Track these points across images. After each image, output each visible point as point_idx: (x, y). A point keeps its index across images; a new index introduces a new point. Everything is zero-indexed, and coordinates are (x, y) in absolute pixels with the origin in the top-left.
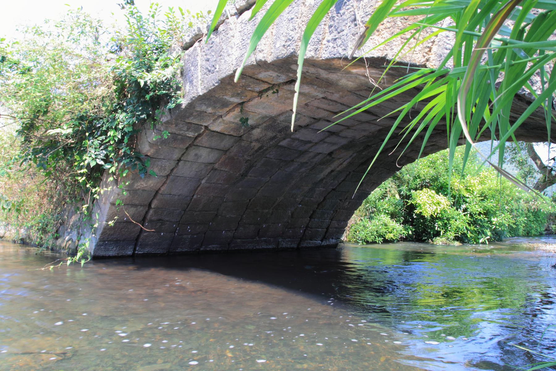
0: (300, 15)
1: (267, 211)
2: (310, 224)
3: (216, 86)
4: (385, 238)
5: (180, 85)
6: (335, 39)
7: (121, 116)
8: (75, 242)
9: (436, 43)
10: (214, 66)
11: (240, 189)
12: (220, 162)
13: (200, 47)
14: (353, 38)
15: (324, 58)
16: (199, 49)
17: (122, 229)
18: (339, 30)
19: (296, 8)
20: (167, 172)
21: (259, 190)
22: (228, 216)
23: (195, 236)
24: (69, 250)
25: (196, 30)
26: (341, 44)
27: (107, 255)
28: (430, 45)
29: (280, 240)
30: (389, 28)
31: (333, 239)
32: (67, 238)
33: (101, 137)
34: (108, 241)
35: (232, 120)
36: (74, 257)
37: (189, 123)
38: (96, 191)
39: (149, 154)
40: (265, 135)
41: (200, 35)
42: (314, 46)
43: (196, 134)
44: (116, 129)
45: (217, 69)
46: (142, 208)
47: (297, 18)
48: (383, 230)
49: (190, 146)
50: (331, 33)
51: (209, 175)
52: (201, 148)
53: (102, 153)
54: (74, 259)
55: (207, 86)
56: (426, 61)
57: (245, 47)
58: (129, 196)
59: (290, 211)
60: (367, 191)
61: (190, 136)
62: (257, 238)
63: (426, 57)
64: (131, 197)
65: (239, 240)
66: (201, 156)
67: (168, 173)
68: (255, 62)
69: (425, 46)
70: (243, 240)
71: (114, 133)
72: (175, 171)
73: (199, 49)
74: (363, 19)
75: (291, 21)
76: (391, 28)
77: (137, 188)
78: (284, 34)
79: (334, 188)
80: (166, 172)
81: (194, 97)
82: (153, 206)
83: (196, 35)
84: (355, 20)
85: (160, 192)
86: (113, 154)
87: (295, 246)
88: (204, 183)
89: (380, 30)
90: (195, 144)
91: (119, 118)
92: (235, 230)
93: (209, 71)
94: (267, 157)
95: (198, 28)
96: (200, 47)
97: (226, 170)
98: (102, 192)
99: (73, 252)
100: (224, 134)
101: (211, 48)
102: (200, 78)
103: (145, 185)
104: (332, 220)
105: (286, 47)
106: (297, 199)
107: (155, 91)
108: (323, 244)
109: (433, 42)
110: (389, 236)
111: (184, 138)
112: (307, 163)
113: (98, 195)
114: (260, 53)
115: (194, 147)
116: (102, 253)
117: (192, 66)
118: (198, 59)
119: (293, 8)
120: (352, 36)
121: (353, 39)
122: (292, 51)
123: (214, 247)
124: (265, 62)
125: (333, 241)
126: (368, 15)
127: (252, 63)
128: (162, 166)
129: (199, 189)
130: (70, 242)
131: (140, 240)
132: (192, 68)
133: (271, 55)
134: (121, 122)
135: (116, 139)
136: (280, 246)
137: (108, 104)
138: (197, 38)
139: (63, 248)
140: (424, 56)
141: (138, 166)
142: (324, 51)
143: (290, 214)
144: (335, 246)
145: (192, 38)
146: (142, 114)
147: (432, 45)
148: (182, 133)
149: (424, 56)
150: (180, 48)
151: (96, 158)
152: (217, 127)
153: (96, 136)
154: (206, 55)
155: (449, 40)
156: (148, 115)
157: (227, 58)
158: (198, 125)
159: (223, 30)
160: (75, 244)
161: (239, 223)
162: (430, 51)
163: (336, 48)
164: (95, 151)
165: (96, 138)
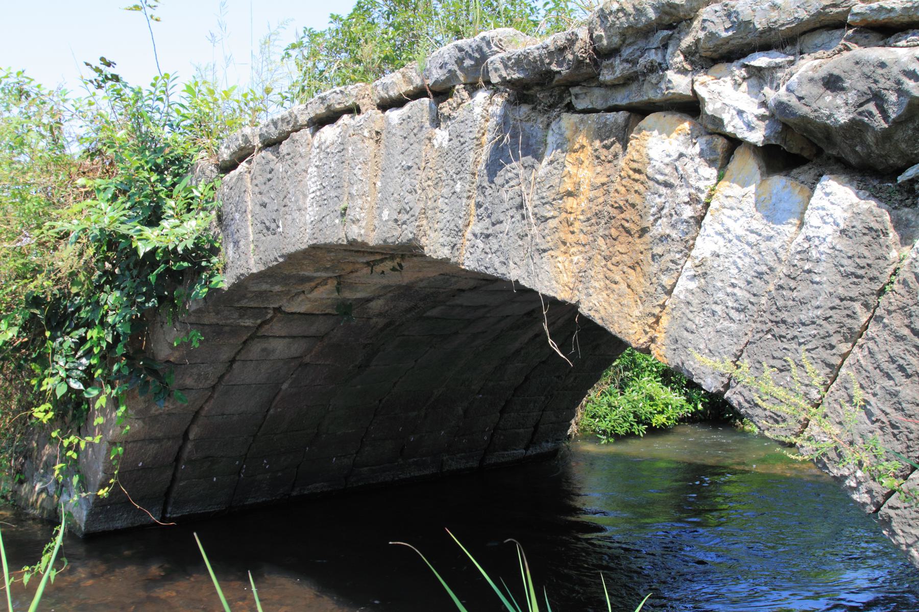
0: (423, 164)
1: (415, 413)
2: (501, 423)
3: (281, 263)
4: (650, 425)
5: (217, 245)
6: (488, 236)
7: (111, 298)
8: (52, 497)
9: (667, 310)
10: (274, 220)
11: (359, 387)
12: (313, 353)
13: (250, 172)
14: (520, 243)
15: (467, 268)
16: (248, 177)
17: (135, 481)
18: (494, 219)
19: (416, 145)
20: (211, 382)
21: (395, 383)
22: (339, 433)
23: (280, 474)
24: (43, 512)
25: (240, 139)
26: (498, 251)
27: (111, 529)
28: (657, 311)
29: (445, 458)
30: (584, 245)
31: (547, 442)
32: (38, 487)
33: (76, 332)
34: (111, 505)
35: (325, 296)
36: (35, 564)
37: (241, 308)
38: (71, 443)
39: (172, 359)
40: (394, 307)
41: (249, 149)
42: (450, 238)
43: (259, 321)
44: (103, 324)
45: (280, 230)
46: (170, 443)
47: (419, 169)
48: (645, 408)
49: (251, 338)
50: (480, 218)
51: (294, 376)
52: (271, 340)
53: (81, 364)
54: (36, 567)
55: (264, 258)
56: (649, 342)
57: (326, 202)
58: (143, 427)
59: (460, 408)
60: (609, 355)
61: (246, 325)
62: (400, 460)
63: (650, 334)
64: (147, 427)
65: (366, 469)
66: (274, 351)
67: (213, 383)
68: (346, 241)
69: (648, 311)
70: (374, 468)
71: (99, 333)
72: (226, 378)
73: (248, 177)
74: (536, 210)
75: (408, 172)
76: (587, 247)
77: (157, 413)
78: (395, 195)
79: (544, 359)
80: (209, 382)
81: (242, 275)
82: (191, 437)
83: (241, 149)
84: (521, 206)
85: (203, 413)
86: (100, 371)
87: (475, 464)
88: (286, 389)
89: (568, 244)
90: (259, 334)
91: (106, 303)
92: (357, 453)
93: (268, 229)
94: (404, 335)
95: (243, 135)
96: (250, 172)
97: (328, 362)
98: (83, 445)
99: (49, 516)
100: (313, 314)
101: (269, 180)
102: (251, 238)
103: (171, 407)
104: (543, 410)
105: (399, 223)
106: (473, 387)
107: (167, 262)
108: (529, 452)
109: (663, 306)
110: (658, 420)
111: (235, 330)
112: (483, 332)
113: (75, 451)
114: (354, 226)
115: (257, 340)
116: (100, 527)
117: (236, 211)
118: (246, 200)
119: (411, 144)
120: (517, 238)
121: (520, 246)
122: (411, 236)
123: (317, 488)
124: (364, 244)
125: (548, 446)
126: (546, 203)
127: (340, 241)
128: (199, 375)
129: (278, 398)
130: (44, 495)
131: (174, 494)
132: (237, 216)
133: (374, 230)
134: (112, 310)
135: (104, 345)
136: (446, 469)
137: (83, 279)
138: (243, 154)
139: (32, 505)
140: (646, 333)
141: (152, 387)
142: (468, 255)
143: (461, 412)
144: (554, 453)
145: (234, 153)
146: (148, 300)
147: (661, 312)
148: (232, 323)
149: (646, 333)
150: (213, 168)
151: (68, 377)
152: (299, 306)
153: (69, 330)
154: (260, 193)
155: (691, 312)
156: (161, 299)
157: (296, 215)
158: (260, 308)
159: (289, 154)
160: (53, 501)
161: (362, 441)
162: (657, 322)
163: (490, 256)
164: (67, 362)
165: (68, 334)
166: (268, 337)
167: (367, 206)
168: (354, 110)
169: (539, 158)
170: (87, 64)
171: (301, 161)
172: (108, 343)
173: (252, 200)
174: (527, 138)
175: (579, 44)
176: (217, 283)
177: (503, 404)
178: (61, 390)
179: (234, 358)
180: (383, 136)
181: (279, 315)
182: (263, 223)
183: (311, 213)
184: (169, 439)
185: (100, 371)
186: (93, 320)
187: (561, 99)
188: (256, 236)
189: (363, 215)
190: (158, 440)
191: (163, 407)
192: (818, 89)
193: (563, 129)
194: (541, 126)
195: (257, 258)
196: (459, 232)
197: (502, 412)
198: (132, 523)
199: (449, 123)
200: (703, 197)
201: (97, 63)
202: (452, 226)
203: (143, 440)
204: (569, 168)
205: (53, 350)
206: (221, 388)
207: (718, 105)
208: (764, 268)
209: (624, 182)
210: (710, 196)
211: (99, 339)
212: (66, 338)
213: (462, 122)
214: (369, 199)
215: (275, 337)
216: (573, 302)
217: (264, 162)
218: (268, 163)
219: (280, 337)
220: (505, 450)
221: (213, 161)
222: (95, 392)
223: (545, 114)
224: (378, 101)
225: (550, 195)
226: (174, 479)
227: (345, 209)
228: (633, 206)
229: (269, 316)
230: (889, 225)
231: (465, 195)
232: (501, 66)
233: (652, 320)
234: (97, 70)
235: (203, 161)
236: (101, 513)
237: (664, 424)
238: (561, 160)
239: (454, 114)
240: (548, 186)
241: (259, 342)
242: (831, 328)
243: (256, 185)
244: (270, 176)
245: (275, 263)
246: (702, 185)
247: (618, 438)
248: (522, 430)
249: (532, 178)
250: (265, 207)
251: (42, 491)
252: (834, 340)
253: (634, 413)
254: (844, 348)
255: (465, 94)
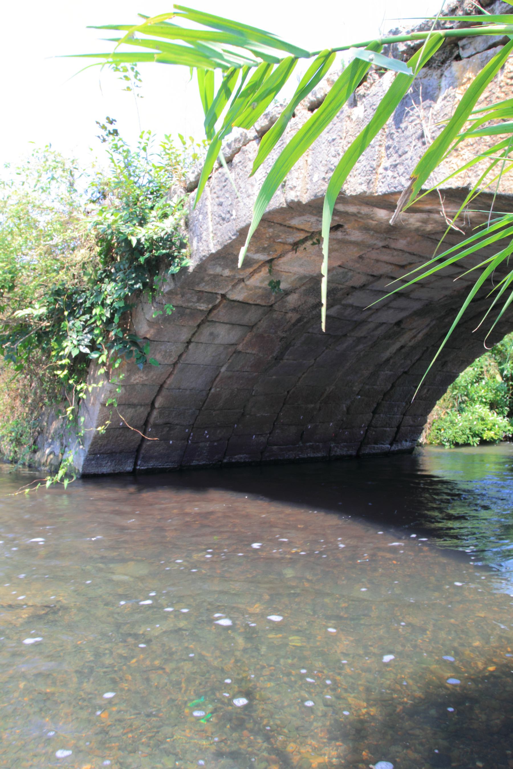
0: (344, 135)
1: (312, 406)
5: (185, 241)
6: (395, 166)
7: (109, 287)
10: (229, 212)
12: (245, 342)
17: (117, 437)
18: (400, 152)
20: (173, 359)
21: (300, 378)
22: (258, 415)
23: (216, 444)
26: (404, 172)
27: (100, 473)
29: (332, 445)
30: (472, 145)
31: (406, 441)
32: (48, 451)
34: (100, 454)
35: (258, 284)
37: (200, 291)
38: (82, 388)
40: (305, 302)
43: (210, 306)
44: (103, 305)
45: (234, 217)
47: (341, 138)
48: (478, 427)
49: (203, 322)
50: (388, 156)
51: (230, 361)
52: (217, 324)
54: (55, 478)
55: (221, 240)
59: (344, 405)
62: (300, 443)
64: (127, 394)
65: (276, 447)
66: (218, 336)
67: (175, 361)
71: (101, 311)
72: (184, 357)
75: (332, 143)
76: (475, 145)
77: (135, 382)
79: (406, 370)
80: (172, 359)
81: (204, 256)
82: (157, 405)
84: (422, 136)
85: (166, 386)
87: (353, 452)
88: (224, 372)
90: (209, 318)
91: (106, 290)
92: (270, 433)
93: (223, 219)
94: (309, 333)
100: (248, 304)
101: (224, 187)
102: (211, 229)
103: (145, 378)
105: (326, 180)
106: (354, 389)
107: (151, 251)
110: (487, 435)
111: (194, 313)
112: (365, 337)
115: (207, 323)
116: (93, 470)
119: (335, 124)
123: (241, 458)
124: (299, 203)
125: (406, 445)
127: (281, 205)
128: (166, 352)
129: (218, 379)
130: (52, 456)
131: (143, 451)
132: (201, 217)
135: (104, 319)
136: (333, 453)
137: (91, 272)
139: (44, 464)
141: (134, 353)
142: (381, 184)
143: (345, 409)
144: (410, 451)
146: (136, 283)
150: (182, 190)
153: (78, 316)
154: (218, 197)
156: (145, 284)
159: (240, 162)
161: (274, 424)
163: (398, 178)
165: (78, 318)
166: (216, 322)
167: (301, 176)
169: (434, 99)
170: (97, 123)
172: (107, 317)
173: (211, 204)
174: (425, 89)
176: (187, 263)
177: (375, 405)
179: (190, 340)
181: (225, 301)
182: (220, 216)
184: (141, 405)
185: (101, 339)
186: (97, 302)
187: (451, 53)
188: (215, 227)
189: (298, 183)
190: (133, 406)
191: (138, 378)
193: (454, 72)
194: (436, 77)
195: (215, 242)
197: (374, 412)
198: (114, 470)
199: (364, 100)
201: (104, 122)
202: (368, 168)
203: (124, 404)
206: (179, 365)
209: (503, 90)
211: (101, 315)
212: (76, 320)
213: (374, 95)
214: (303, 171)
216: (465, 185)
217: (220, 176)
220: (376, 443)
221: (182, 184)
223: (438, 69)
224: (309, 105)
229: (218, 301)
231: (378, 143)
234: (104, 127)
236: (93, 460)
237: (492, 438)
238: (452, 94)
239: (368, 92)
240: (442, 115)
241: (208, 326)
243: (215, 193)
245: (229, 241)
247: (457, 445)
248: (388, 429)
249: (430, 114)
250: (221, 205)
251: (50, 453)
253: (470, 429)
255: (376, 76)
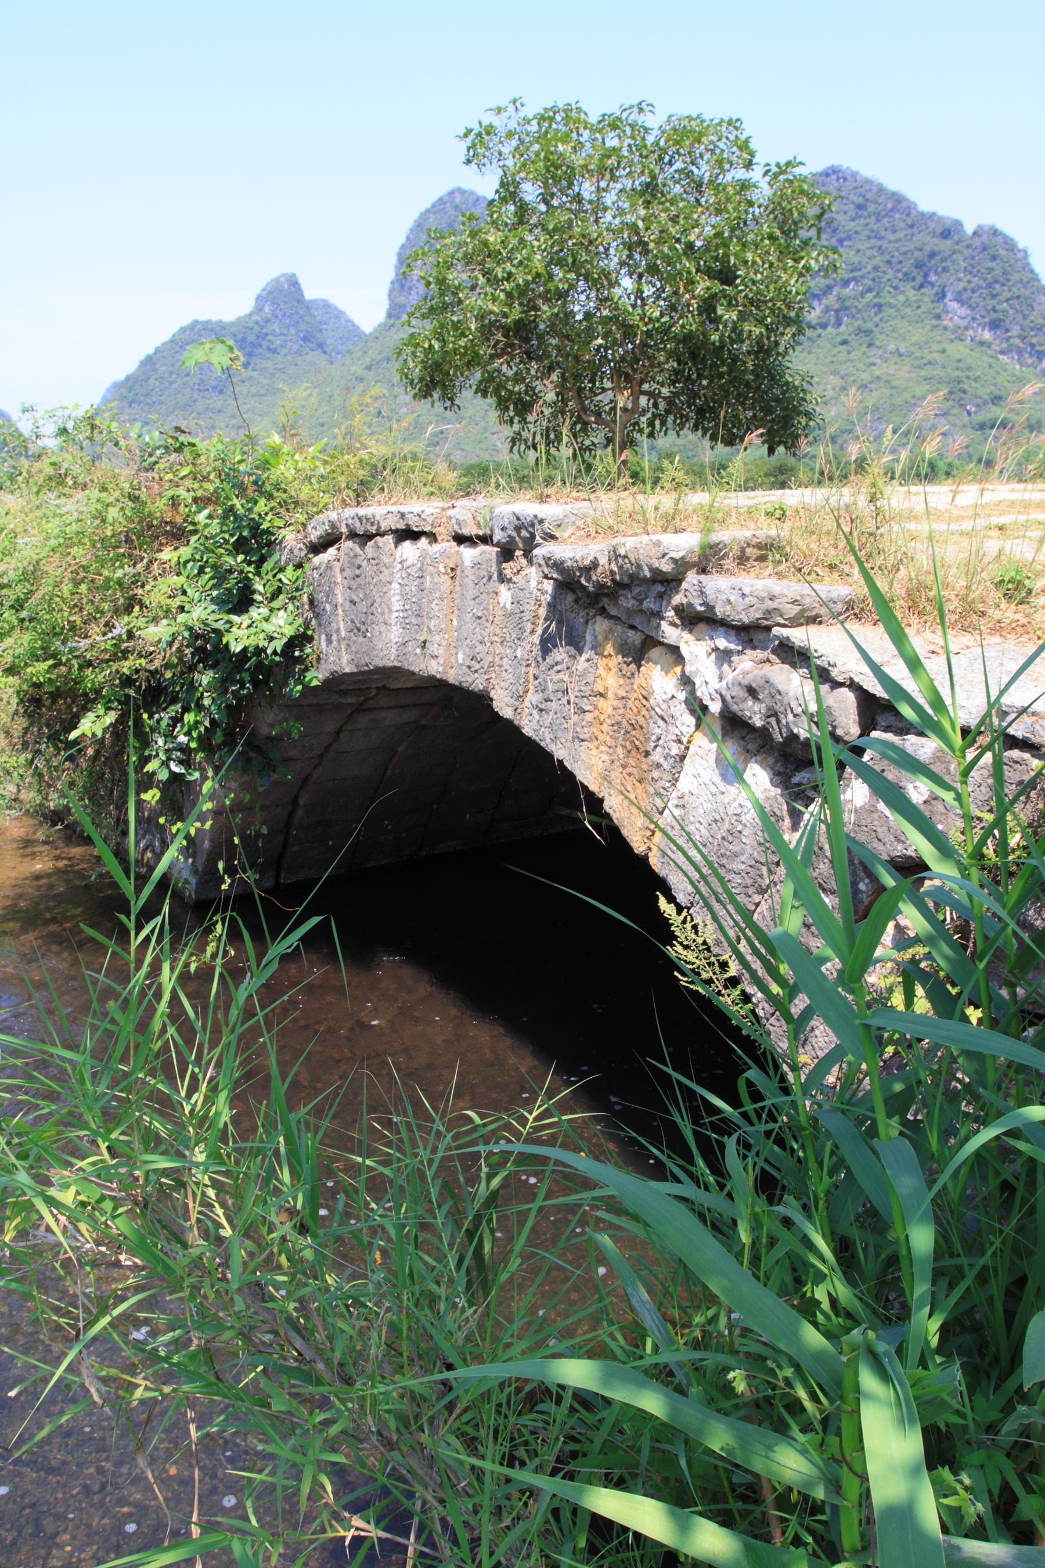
5: (310, 633)
6: (541, 710)
82: (301, 802)
132: (328, 607)
135: (202, 729)
157: (383, 628)
165: (164, 709)
168: (432, 537)
169: (580, 651)
171: (386, 572)
175: (599, 570)
176: (311, 680)
178: (163, 776)
180: (458, 572)
182: (352, 621)
183: (395, 634)
192: (743, 694)
196: (520, 698)
200: (685, 740)
204: (601, 671)
205: (151, 728)
207: (693, 669)
208: (718, 817)
210: (689, 742)
211: (197, 722)
215: (382, 708)
218: (356, 556)
219: (388, 708)
222: (197, 775)
225: (587, 690)
226: (285, 845)
227: (425, 642)
228: (641, 727)
230: (785, 814)
232: (543, 563)
233: (649, 833)
235: (291, 539)
242: (749, 882)
244: (358, 572)
246: (685, 729)
252: (751, 891)
254: (757, 898)
